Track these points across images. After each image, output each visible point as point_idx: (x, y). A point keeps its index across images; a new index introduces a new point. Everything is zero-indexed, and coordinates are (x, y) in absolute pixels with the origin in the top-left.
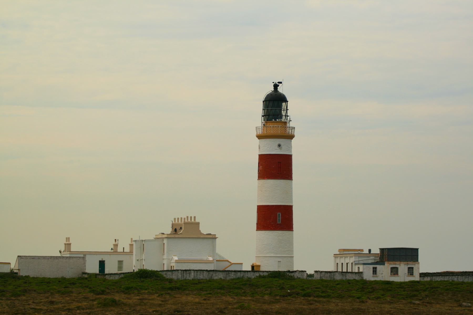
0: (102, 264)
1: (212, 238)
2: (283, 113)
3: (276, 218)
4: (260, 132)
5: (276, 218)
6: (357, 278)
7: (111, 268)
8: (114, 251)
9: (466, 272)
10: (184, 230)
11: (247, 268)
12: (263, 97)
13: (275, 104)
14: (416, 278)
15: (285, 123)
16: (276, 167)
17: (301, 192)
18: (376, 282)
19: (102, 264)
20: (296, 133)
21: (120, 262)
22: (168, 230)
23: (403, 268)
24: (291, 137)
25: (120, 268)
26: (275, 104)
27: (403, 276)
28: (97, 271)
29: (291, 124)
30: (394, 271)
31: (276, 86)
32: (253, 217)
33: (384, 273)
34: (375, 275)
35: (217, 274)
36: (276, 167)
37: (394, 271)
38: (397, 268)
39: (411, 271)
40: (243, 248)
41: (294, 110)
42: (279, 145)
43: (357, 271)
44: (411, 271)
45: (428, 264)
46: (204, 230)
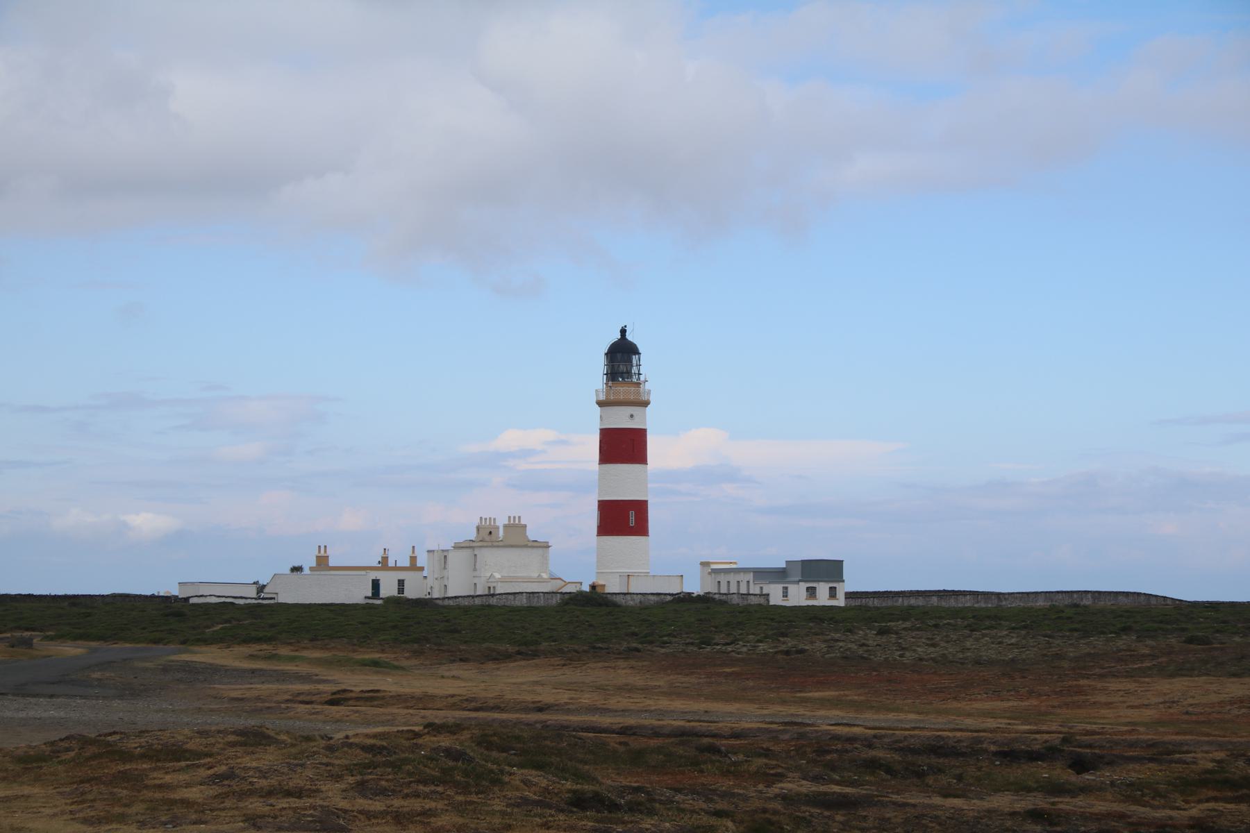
2: (634, 370)
4: (602, 397)
5: (621, 518)
6: (762, 601)
8: (384, 564)
9: (918, 592)
11: (586, 588)
12: (605, 348)
13: (622, 356)
14: (840, 602)
15: (638, 384)
16: (623, 446)
18: (785, 607)
20: (652, 399)
21: (401, 583)
22: (472, 535)
23: (823, 589)
24: (645, 404)
25: (401, 590)
26: (622, 356)
27: (823, 599)
29: (648, 386)
30: (812, 592)
31: (623, 331)
32: (592, 519)
33: (797, 596)
34: (622, 391)
36: (623, 446)
37: (812, 592)
38: (814, 588)
40: (576, 558)
41: (648, 366)
42: (632, 416)
43: (758, 592)
44: (833, 593)
45: (856, 580)
46: (531, 535)
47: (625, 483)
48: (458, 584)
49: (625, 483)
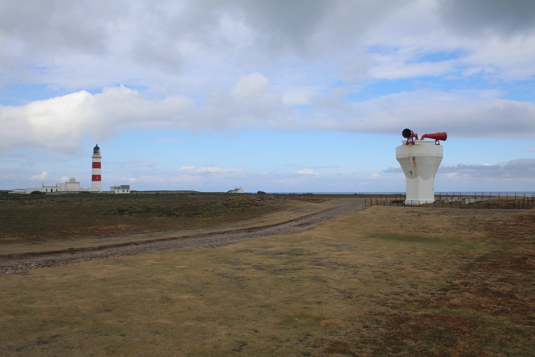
0: (52, 190)
1: (79, 183)
3: (96, 178)
5: (96, 178)
7: (54, 190)
10: (73, 181)
13: (96, 149)
14: (129, 192)
16: (96, 165)
17: (101, 171)
19: (52, 190)
23: (126, 190)
26: (96, 149)
27: (126, 192)
28: (50, 191)
30: (123, 191)
32: (91, 178)
33: (121, 192)
34: (96, 155)
35: (132, 246)
36: (96, 165)
37: (123, 191)
39: (128, 191)
41: (101, 151)
44: (128, 191)
45: (131, 189)
46: (77, 181)
47: (97, 172)
48: (63, 189)
49: (97, 172)
